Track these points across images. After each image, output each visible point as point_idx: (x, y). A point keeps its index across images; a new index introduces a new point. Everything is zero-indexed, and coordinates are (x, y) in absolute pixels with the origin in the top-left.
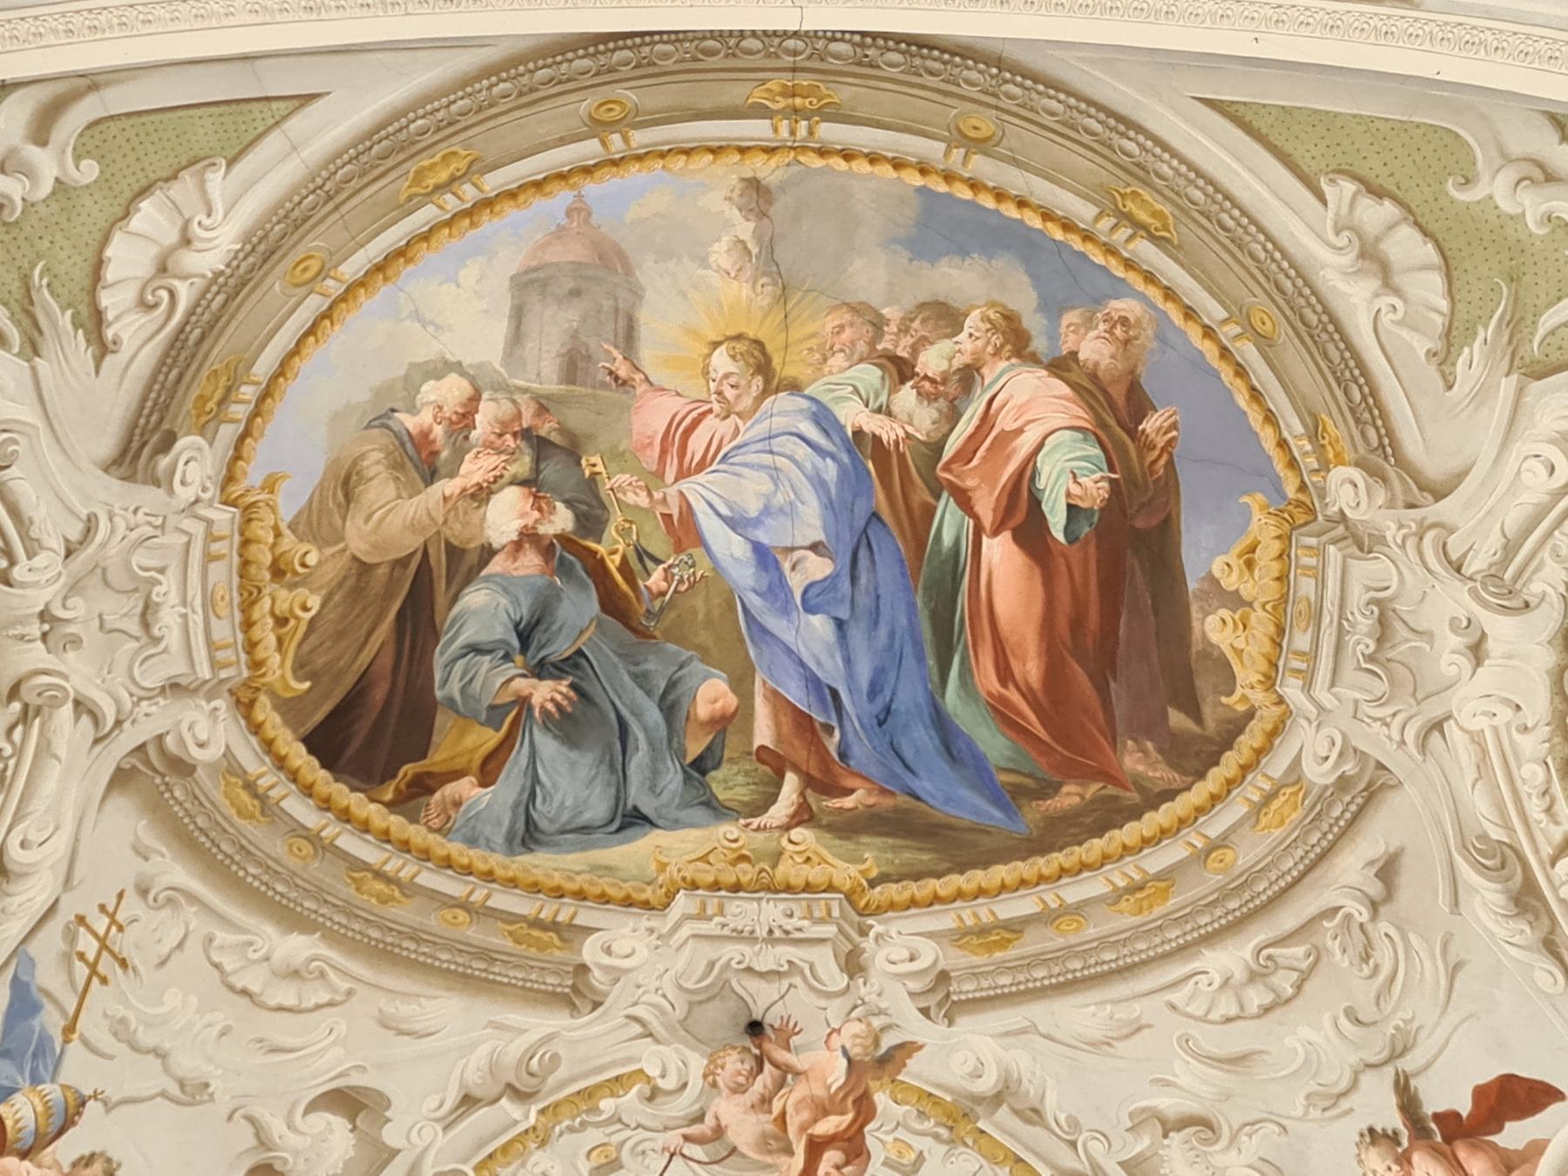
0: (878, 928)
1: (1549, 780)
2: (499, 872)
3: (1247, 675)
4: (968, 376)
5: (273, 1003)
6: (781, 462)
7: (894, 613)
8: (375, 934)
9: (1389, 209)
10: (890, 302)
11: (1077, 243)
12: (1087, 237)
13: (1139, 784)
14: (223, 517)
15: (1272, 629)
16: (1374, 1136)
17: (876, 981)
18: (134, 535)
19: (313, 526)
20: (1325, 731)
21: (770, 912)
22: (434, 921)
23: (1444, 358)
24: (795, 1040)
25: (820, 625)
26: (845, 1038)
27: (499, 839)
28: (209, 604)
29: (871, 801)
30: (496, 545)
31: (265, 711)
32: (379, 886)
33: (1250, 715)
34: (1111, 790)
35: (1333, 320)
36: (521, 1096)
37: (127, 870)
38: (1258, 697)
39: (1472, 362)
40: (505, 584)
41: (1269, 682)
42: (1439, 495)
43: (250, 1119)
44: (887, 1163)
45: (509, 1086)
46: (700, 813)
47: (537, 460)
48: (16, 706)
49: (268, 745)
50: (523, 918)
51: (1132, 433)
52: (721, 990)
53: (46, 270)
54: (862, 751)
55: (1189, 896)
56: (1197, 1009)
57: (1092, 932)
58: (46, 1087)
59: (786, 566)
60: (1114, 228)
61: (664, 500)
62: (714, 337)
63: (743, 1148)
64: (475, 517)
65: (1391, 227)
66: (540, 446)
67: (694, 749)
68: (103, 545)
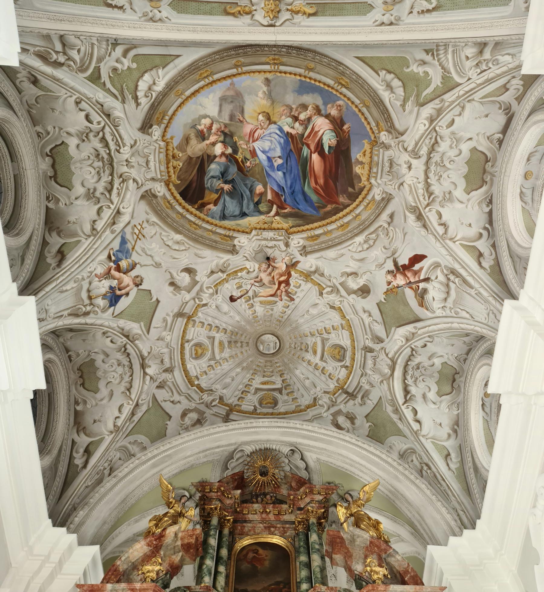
0: (292, 237)
1: (424, 192)
2: (218, 225)
3: (364, 179)
4: (309, 119)
5: (174, 248)
6: (273, 139)
7: (295, 171)
8: (194, 236)
9: (392, 76)
10: (294, 104)
11: (330, 90)
12: (333, 88)
13: (342, 204)
14: (162, 144)
15: (369, 168)
16: (389, 272)
17: (291, 248)
18: (144, 145)
19: (182, 147)
20: (379, 189)
21: (271, 234)
22: (205, 234)
23: (403, 106)
24: (276, 261)
25: (280, 173)
26: (285, 261)
27: (218, 218)
28: (160, 162)
29: (290, 210)
30: (217, 155)
31: (171, 186)
32: (195, 226)
33: (364, 187)
34: (337, 206)
35: (381, 101)
36: (223, 272)
37: (144, 217)
38: (366, 183)
39: (409, 105)
40: (219, 164)
41: (368, 179)
42: (402, 134)
43: (170, 272)
44: (294, 286)
45: (220, 270)
46: (257, 213)
47: (225, 137)
48: (121, 179)
49: (172, 194)
50: (223, 234)
51: (342, 130)
52: (261, 251)
53: (126, 85)
54: (289, 200)
55: (352, 226)
56: (354, 250)
57: (333, 236)
58: (129, 260)
59: (274, 161)
60: (338, 86)
61: (250, 147)
62: (259, 112)
63: (266, 283)
64: (212, 149)
65: (393, 79)
66: (225, 134)
67: (256, 200)
68: (138, 146)
